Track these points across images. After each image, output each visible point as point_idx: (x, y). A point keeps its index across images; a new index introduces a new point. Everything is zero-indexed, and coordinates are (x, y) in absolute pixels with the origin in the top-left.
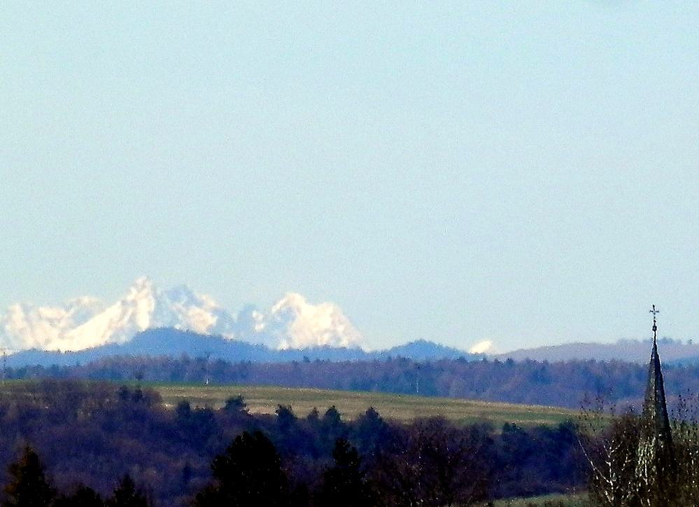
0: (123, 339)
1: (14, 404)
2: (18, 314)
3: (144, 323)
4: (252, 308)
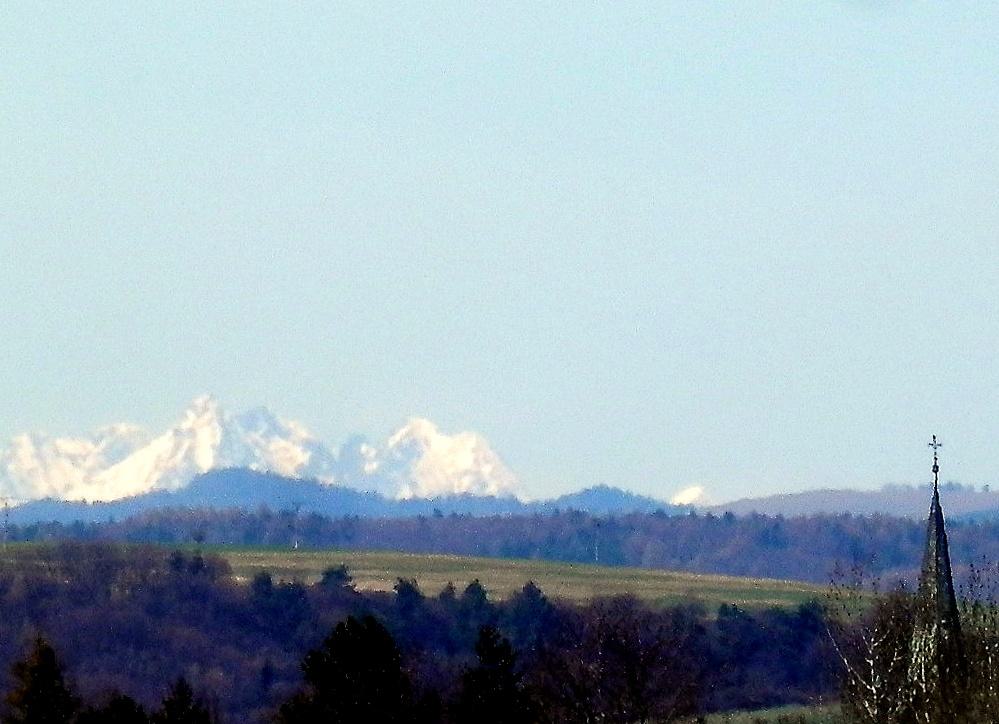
0: (176, 484)
1: (19, 577)
2: (26, 449)
3: (206, 462)
4: (360, 439)
